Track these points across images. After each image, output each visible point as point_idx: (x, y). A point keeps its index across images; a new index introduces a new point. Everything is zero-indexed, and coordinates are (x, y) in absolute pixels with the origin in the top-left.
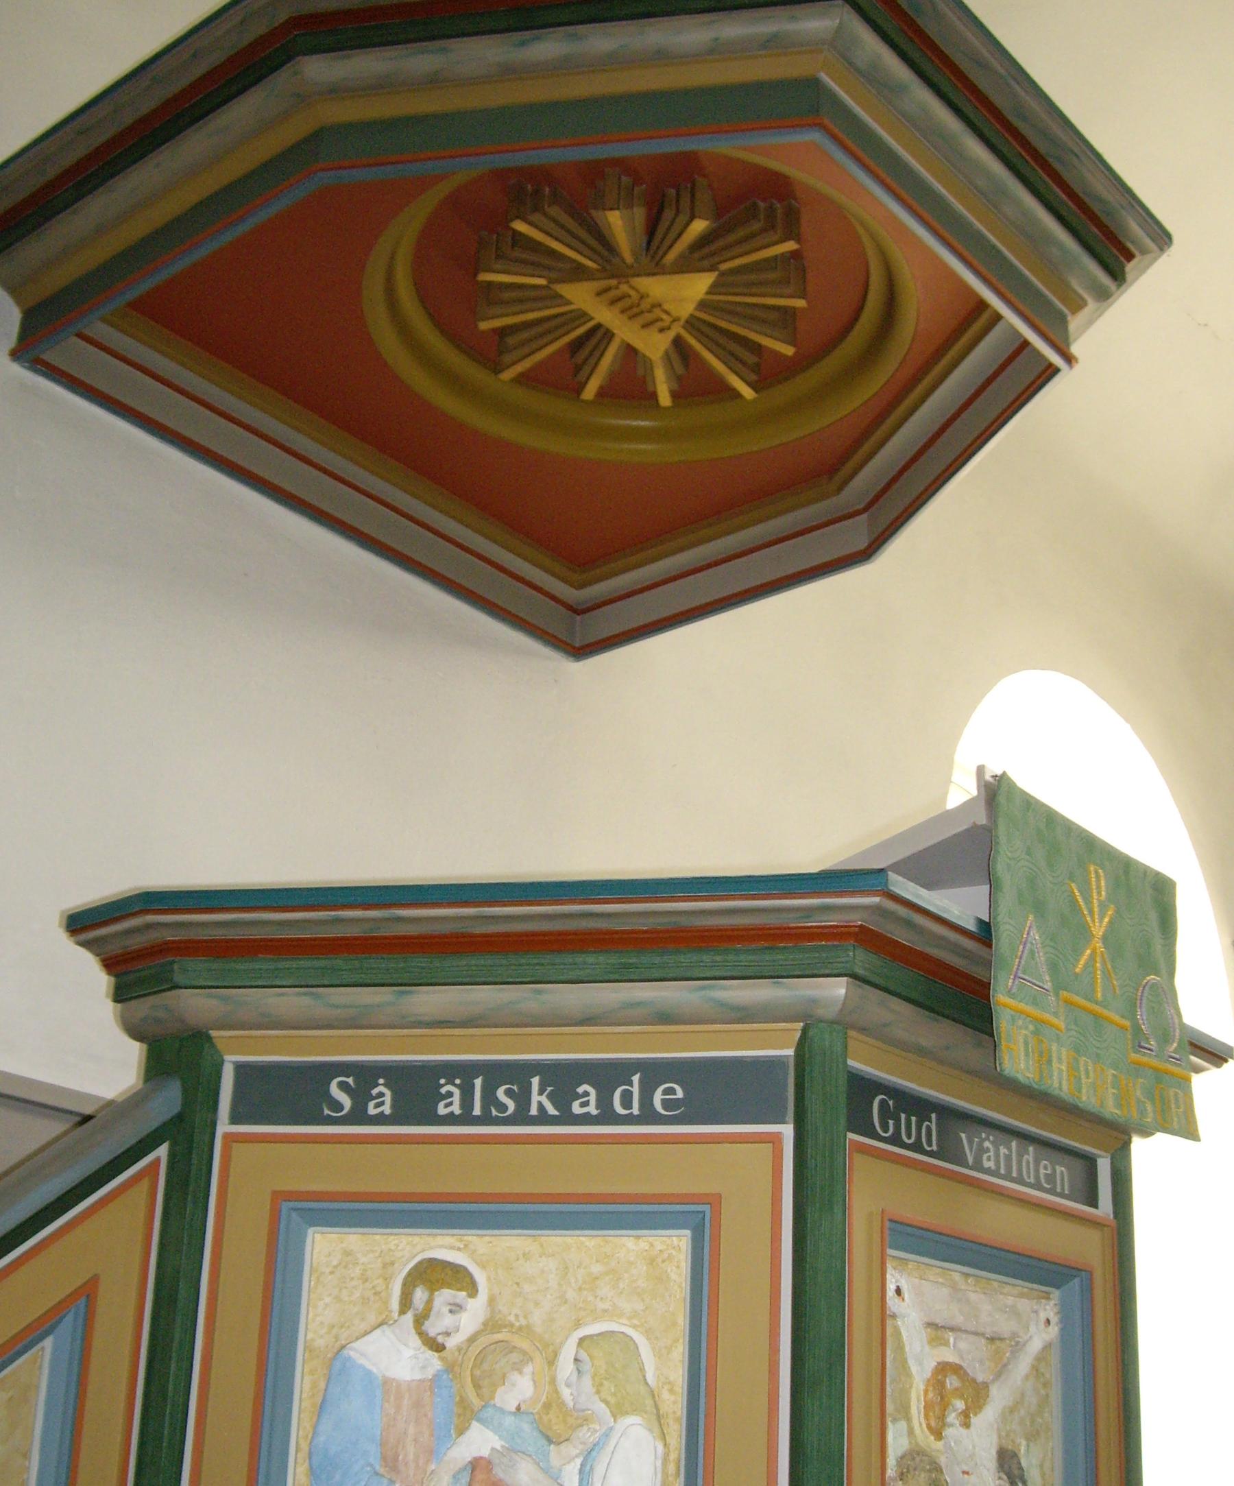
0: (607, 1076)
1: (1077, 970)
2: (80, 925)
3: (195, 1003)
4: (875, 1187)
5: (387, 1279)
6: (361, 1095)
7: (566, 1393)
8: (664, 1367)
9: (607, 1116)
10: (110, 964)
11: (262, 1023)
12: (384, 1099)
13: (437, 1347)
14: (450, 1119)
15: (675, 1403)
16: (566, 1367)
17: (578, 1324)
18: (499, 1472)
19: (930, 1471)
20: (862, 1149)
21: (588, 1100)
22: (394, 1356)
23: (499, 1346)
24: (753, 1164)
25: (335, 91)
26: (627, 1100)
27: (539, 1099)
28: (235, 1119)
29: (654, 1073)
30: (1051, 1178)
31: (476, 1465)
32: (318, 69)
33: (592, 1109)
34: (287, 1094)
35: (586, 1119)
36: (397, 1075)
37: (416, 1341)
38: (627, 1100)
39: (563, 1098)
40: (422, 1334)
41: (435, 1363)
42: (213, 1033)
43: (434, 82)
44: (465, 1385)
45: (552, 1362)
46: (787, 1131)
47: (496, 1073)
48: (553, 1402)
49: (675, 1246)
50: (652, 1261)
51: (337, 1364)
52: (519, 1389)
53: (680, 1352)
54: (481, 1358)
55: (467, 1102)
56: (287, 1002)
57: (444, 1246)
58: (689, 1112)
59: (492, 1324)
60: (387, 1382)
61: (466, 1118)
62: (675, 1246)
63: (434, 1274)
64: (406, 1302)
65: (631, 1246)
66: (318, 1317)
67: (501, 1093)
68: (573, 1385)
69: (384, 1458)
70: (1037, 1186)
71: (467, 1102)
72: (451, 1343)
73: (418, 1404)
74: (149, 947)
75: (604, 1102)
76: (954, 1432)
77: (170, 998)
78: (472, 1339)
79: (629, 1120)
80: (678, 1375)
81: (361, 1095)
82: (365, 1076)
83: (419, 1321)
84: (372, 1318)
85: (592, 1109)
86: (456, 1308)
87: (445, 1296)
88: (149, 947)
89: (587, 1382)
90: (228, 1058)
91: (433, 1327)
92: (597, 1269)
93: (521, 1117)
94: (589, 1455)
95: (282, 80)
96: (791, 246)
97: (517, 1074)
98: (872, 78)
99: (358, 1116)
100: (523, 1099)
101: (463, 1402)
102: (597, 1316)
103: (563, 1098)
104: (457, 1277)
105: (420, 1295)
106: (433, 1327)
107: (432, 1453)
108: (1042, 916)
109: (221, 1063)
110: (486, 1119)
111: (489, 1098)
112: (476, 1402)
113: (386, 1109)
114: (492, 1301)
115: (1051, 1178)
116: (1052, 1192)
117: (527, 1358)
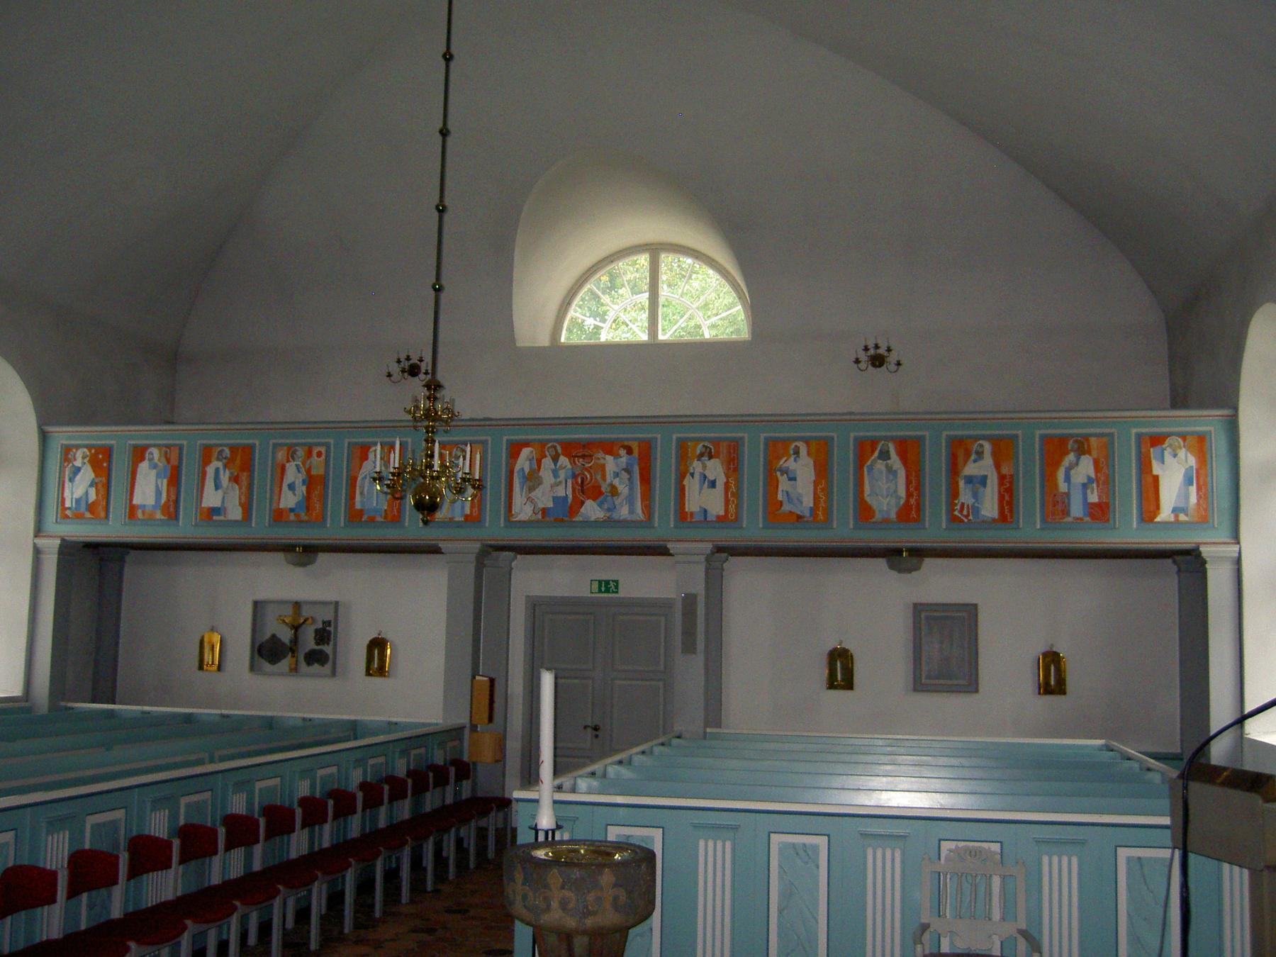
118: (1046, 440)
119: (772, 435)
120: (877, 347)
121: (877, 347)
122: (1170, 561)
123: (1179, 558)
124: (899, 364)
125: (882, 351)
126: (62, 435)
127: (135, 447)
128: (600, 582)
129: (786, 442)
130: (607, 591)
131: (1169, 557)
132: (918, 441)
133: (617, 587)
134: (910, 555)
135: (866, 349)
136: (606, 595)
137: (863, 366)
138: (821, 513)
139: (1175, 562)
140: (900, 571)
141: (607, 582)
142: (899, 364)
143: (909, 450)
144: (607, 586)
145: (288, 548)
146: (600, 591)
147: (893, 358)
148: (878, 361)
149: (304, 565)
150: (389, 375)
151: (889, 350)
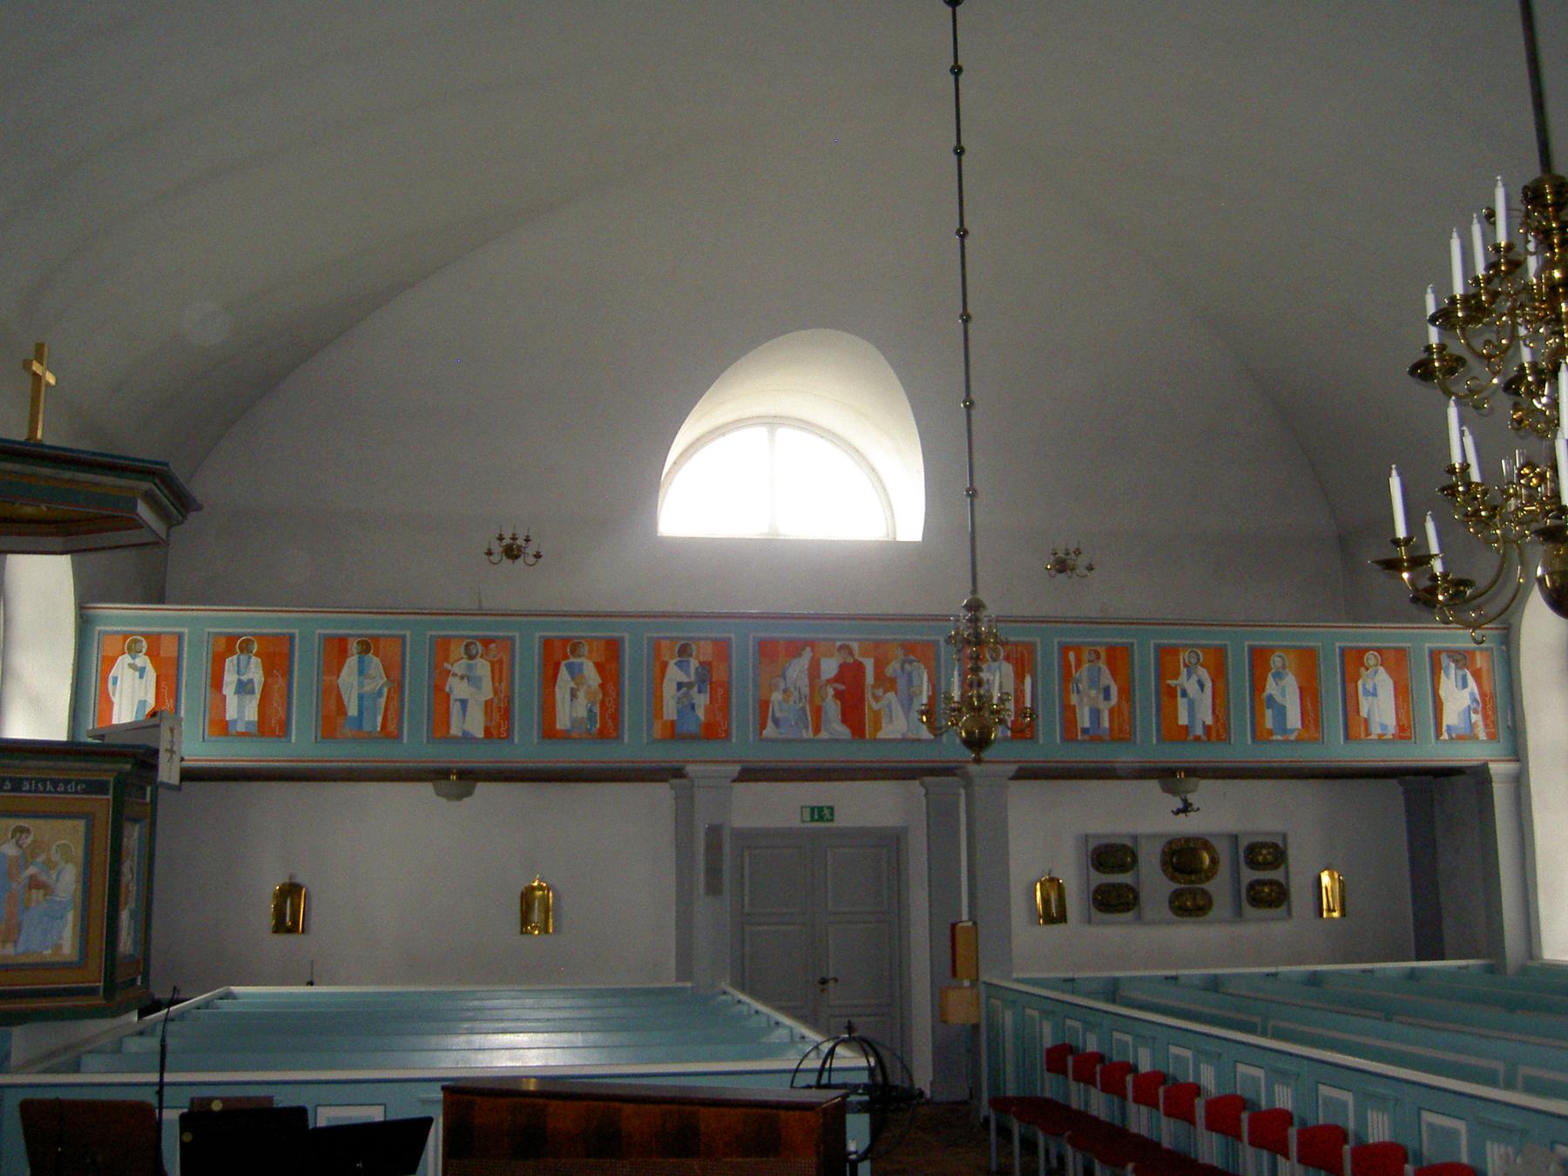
1: (128, 767)
8: (79, 852)
9: (66, 792)
16: (53, 851)
19: (471, 657)
21: (61, 788)
24: (102, 804)
27: (49, 787)
39: (55, 787)
42: (690, 768)
49: (81, 825)
57: (22, 823)
58: (85, 792)
59: (34, 841)
62: (81, 825)
65: (69, 823)
68: (56, 857)
93: (44, 791)
97: (44, 781)
103: (55, 787)
104: (28, 831)
108: (1192, 872)
118: (1343, 652)
119: (627, 644)
120: (514, 539)
121: (514, 539)
122: (1395, 781)
123: (928, 779)
124: (538, 556)
125: (520, 542)
126: (117, 616)
127: (328, 639)
128: (812, 809)
129: (1361, 652)
130: (821, 819)
131: (913, 778)
132: (1127, 649)
133: (832, 814)
134: (459, 778)
135: (501, 538)
136: (814, 825)
137: (495, 558)
138: (1218, 732)
139: (922, 785)
140: (1165, 791)
141: (821, 809)
142: (538, 556)
143: (1118, 658)
144: (820, 813)
145: (436, 775)
146: (813, 820)
147: (531, 550)
148: (512, 553)
149: (460, 797)
150: (489, 553)
151: (527, 540)
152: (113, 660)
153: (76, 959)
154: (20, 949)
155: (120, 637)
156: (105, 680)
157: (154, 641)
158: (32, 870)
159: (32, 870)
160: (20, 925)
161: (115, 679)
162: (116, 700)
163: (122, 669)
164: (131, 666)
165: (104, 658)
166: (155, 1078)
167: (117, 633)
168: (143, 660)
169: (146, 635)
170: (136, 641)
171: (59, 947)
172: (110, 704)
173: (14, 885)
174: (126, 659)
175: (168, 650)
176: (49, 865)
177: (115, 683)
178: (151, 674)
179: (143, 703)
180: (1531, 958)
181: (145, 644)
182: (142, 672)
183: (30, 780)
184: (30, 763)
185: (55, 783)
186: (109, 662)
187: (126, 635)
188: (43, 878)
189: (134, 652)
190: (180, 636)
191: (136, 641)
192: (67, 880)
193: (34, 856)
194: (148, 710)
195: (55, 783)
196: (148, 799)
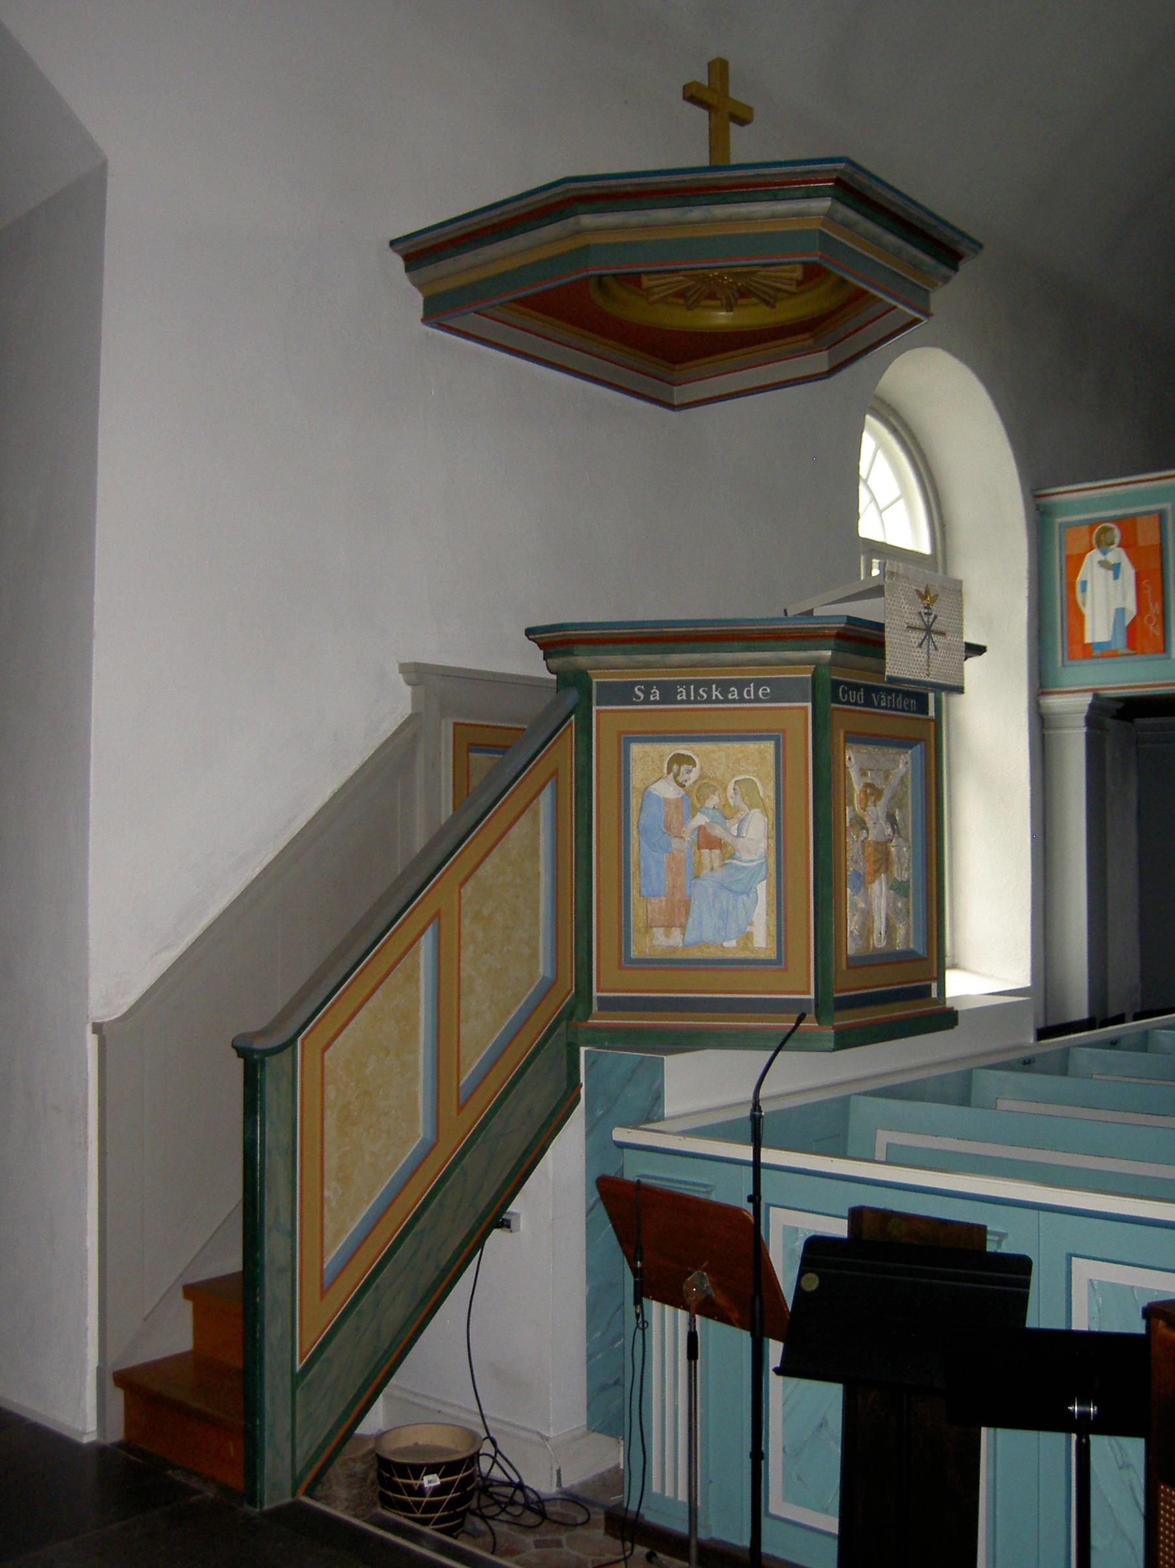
0: (741, 685)
2: (529, 632)
3: (582, 660)
4: (845, 716)
5: (662, 762)
6: (647, 693)
7: (731, 801)
8: (766, 791)
9: (742, 700)
10: (541, 646)
11: (605, 668)
12: (656, 695)
13: (683, 786)
14: (682, 702)
15: (771, 804)
16: (730, 792)
17: (734, 776)
18: (708, 830)
20: (837, 709)
21: (734, 694)
22: (666, 790)
23: (705, 786)
24: (799, 713)
25: (597, 230)
26: (749, 693)
28: (598, 704)
29: (759, 684)
30: (908, 705)
31: (700, 828)
32: (587, 220)
33: (736, 697)
34: (621, 693)
35: (734, 701)
36: (659, 684)
37: (673, 782)
38: (749, 693)
39: (725, 692)
40: (677, 782)
41: (682, 792)
43: (645, 226)
44: (694, 798)
45: (725, 790)
46: (809, 705)
47: (698, 684)
48: (726, 805)
49: (769, 747)
50: (760, 753)
51: (645, 793)
52: (714, 801)
53: (772, 785)
54: (699, 790)
55: (688, 695)
56: (619, 659)
57: (683, 749)
59: (702, 777)
60: (665, 800)
61: (688, 701)
62: (769, 747)
63: (679, 759)
64: (669, 770)
65: (752, 746)
66: (637, 777)
67: (701, 691)
69: (666, 827)
70: (903, 710)
71: (688, 695)
72: (687, 784)
73: (677, 807)
74: (553, 641)
75: (740, 694)
76: (870, 808)
77: (572, 659)
78: (695, 782)
79: (750, 701)
80: (772, 794)
81: (647, 693)
82: (648, 686)
83: (675, 777)
84: (657, 776)
85: (736, 697)
86: (689, 772)
87: (684, 768)
88: (553, 641)
89: (739, 797)
90: (594, 680)
91: (680, 779)
92: (740, 755)
93: (709, 700)
94: (742, 821)
95: (569, 223)
96: (990, 955)
97: (707, 684)
98: (847, 225)
99: (646, 701)
100: (709, 693)
101: (693, 805)
102: (741, 773)
103: (725, 692)
104: (689, 760)
105: (675, 767)
106: (680, 779)
107: (683, 824)
109: (591, 682)
110: (696, 702)
111: (697, 693)
112: (698, 805)
113: (658, 698)
114: (702, 768)
115: (908, 705)
116: (909, 711)
117: (716, 789)
152: (1080, 558)
153: (773, 956)
154: (691, 936)
155: (1085, 528)
156: (1071, 587)
157: (1127, 524)
158: (700, 820)
159: (700, 820)
160: (687, 905)
161: (1084, 583)
162: (1087, 611)
163: (1092, 570)
164: (1104, 564)
165: (1069, 558)
166: (768, 1156)
167: (1081, 523)
168: (1116, 555)
169: (1117, 521)
170: (1106, 530)
171: (749, 937)
172: (1080, 617)
173: (676, 843)
174: (1094, 556)
175: (1147, 536)
176: (726, 812)
177: (1084, 590)
178: (1128, 572)
179: (1121, 612)
180: (463, 1532)
181: (1117, 532)
182: (1116, 569)
183: (687, 684)
184: (675, 658)
185: (724, 686)
186: (1075, 562)
187: (1093, 524)
188: (717, 832)
189: (1103, 544)
190: (1161, 516)
191: (1106, 530)
192: (754, 835)
193: (702, 798)
194: (1128, 621)
195: (724, 686)
196: (932, 713)
